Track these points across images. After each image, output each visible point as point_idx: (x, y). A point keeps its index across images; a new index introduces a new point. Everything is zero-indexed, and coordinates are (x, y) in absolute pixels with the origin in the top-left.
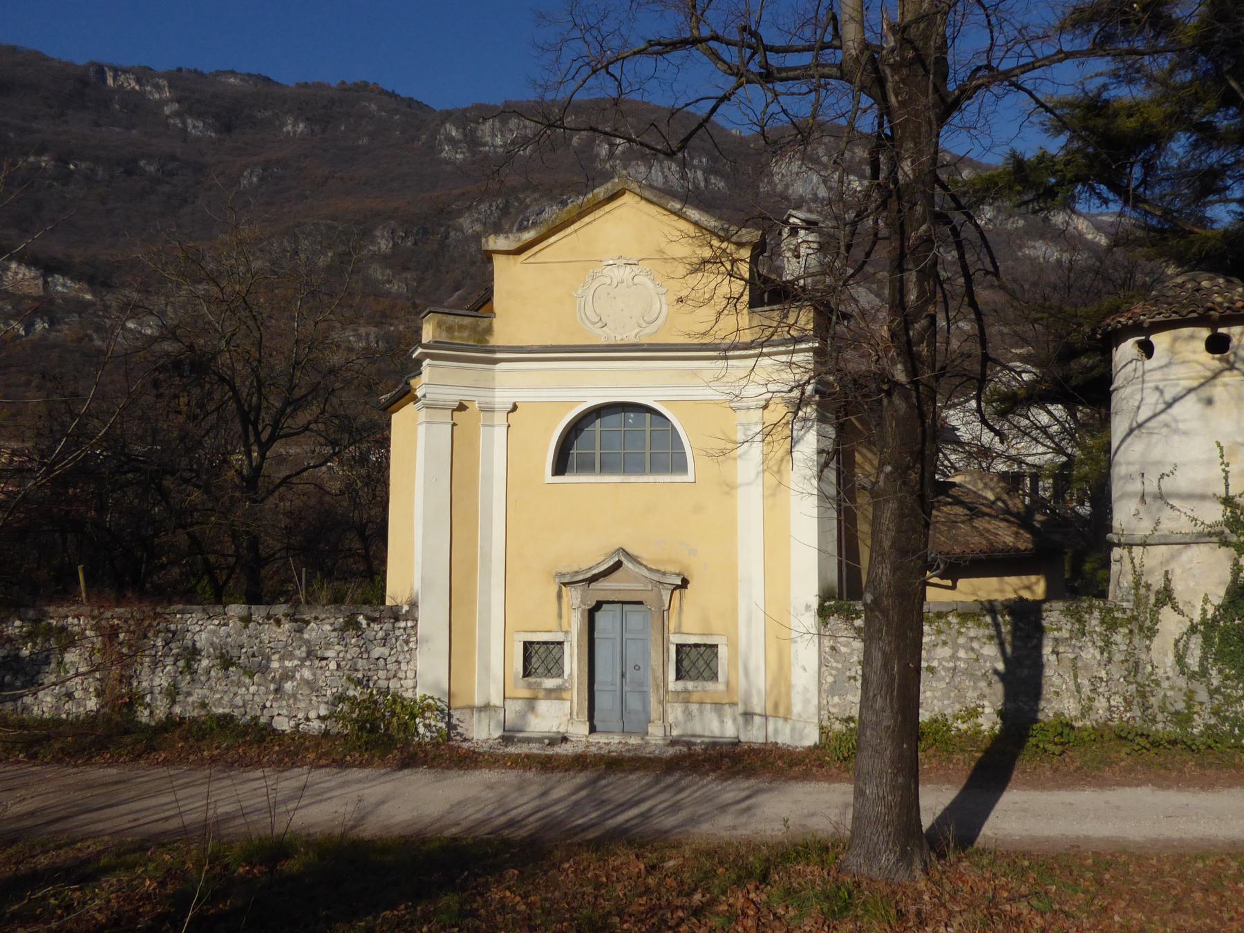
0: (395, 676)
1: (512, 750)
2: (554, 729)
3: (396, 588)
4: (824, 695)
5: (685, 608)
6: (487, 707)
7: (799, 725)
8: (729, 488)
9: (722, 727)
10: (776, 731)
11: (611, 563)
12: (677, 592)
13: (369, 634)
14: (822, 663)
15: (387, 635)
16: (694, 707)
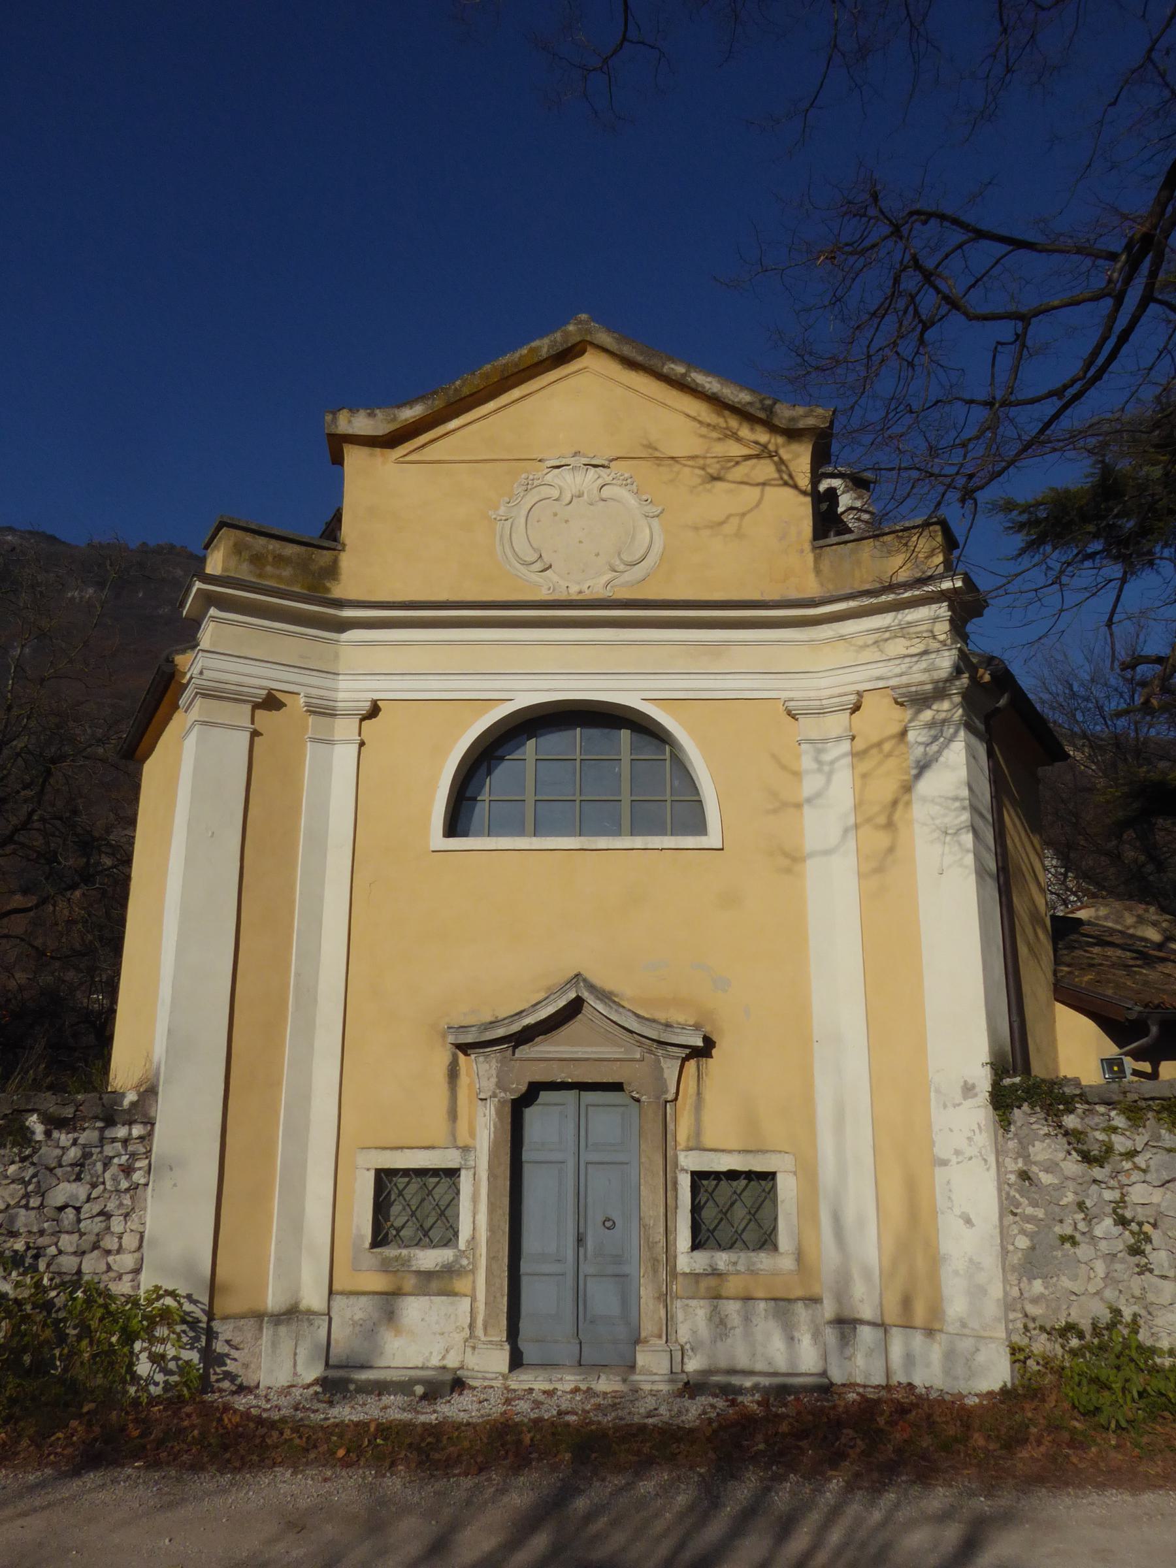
0: (96, 1246)
1: (344, 1413)
2: (435, 1361)
3: (125, 1068)
4: (1013, 1278)
5: (708, 1096)
6: (292, 1314)
7: (966, 1345)
8: (791, 860)
9: (788, 1351)
10: (909, 1359)
11: (562, 1003)
12: (691, 1065)
13: (49, 1153)
14: (1008, 1208)
15: (86, 1155)
16: (732, 1308)
